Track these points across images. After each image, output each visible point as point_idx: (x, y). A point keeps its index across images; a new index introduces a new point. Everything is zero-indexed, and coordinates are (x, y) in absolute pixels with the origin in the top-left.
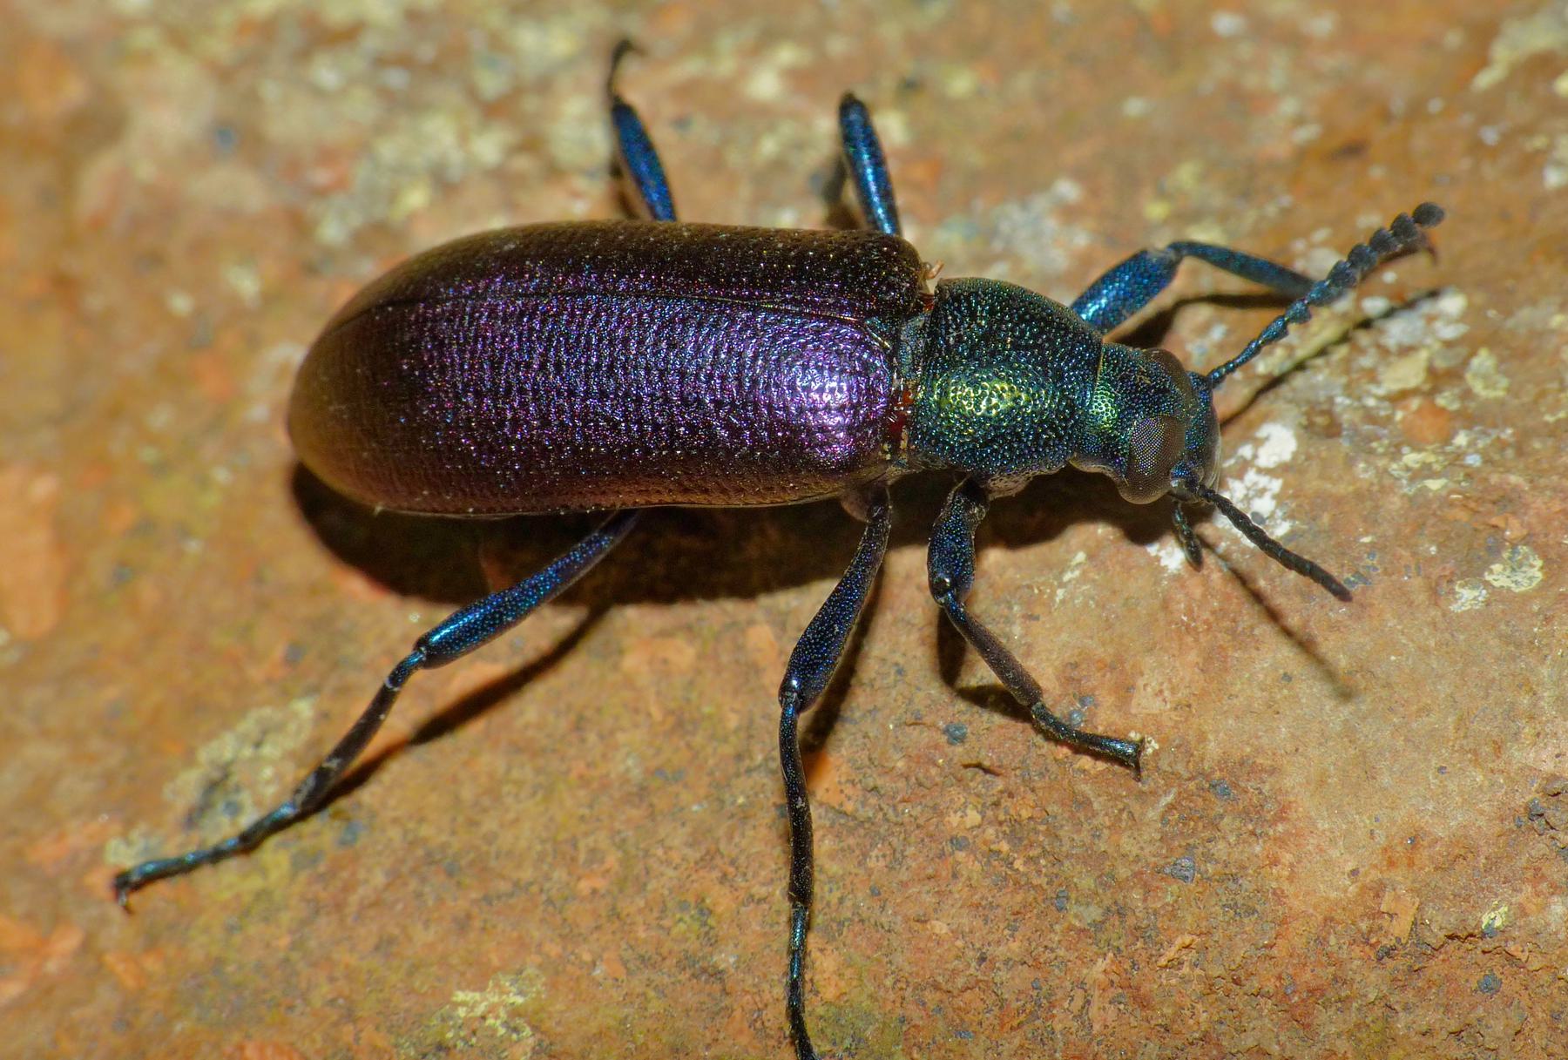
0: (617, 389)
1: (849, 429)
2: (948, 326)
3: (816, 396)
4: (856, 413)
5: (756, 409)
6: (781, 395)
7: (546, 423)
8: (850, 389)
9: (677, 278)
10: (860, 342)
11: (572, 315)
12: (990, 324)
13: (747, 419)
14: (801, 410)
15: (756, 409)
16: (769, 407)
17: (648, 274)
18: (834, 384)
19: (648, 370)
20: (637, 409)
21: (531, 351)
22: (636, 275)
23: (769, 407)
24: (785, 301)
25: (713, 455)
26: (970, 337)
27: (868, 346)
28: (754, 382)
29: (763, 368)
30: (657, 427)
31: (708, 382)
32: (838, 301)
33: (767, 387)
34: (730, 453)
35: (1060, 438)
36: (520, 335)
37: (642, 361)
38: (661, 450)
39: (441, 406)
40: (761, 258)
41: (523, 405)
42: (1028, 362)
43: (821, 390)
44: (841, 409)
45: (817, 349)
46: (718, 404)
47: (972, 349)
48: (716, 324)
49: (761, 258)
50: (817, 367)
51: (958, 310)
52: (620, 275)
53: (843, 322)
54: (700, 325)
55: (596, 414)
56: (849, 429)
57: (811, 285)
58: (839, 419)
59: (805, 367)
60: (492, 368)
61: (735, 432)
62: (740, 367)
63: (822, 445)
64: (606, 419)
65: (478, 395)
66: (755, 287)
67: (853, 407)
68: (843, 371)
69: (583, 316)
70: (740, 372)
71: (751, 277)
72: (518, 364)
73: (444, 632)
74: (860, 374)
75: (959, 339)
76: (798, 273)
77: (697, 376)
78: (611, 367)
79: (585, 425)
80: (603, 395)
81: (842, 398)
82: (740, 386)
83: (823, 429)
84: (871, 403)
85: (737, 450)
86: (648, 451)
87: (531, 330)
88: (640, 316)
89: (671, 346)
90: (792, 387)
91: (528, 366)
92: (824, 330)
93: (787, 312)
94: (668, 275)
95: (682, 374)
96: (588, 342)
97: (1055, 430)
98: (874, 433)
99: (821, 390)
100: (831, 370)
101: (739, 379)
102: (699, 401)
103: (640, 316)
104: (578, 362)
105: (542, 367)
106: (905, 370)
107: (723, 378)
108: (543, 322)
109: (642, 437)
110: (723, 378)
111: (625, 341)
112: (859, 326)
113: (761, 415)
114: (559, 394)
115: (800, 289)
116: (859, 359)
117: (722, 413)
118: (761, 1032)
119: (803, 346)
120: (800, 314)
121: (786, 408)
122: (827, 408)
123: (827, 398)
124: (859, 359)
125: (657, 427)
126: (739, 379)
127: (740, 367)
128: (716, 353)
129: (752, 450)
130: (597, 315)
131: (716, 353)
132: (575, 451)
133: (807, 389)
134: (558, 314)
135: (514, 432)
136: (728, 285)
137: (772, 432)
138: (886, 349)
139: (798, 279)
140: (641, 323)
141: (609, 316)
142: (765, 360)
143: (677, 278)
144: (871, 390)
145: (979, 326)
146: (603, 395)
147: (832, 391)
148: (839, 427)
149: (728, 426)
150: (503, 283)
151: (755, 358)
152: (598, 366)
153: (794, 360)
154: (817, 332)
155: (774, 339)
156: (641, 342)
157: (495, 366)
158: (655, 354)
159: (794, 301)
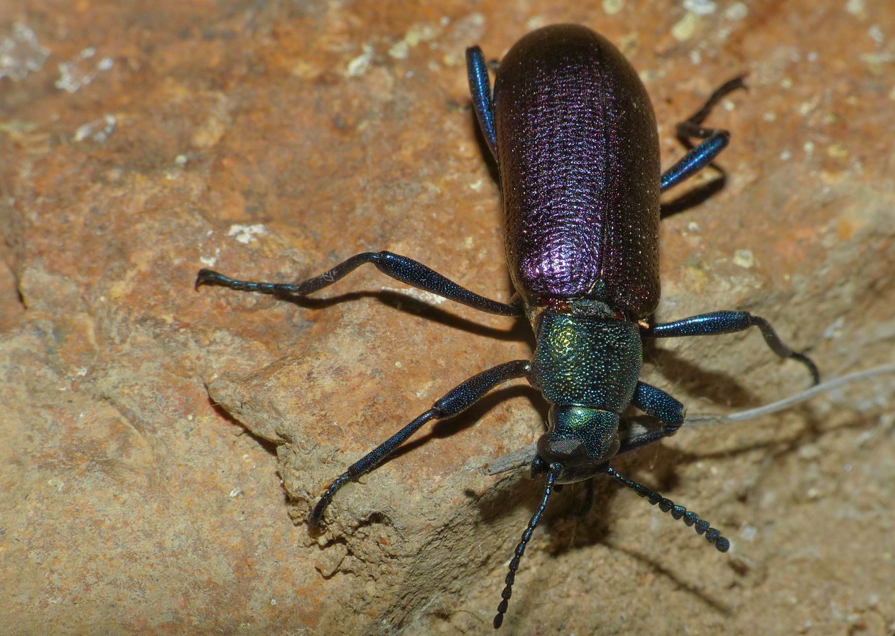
0: (555, 157)
1: (541, 275)
2: (612, 328)
3: (557, 255)
4: (550, 278)
5: (548, 226)
6: (556, 238)
7: (535, 126)
8: (563, 273)
9: (619, 183)
10: (590, 277)
11: (594, 132)
12: (617, 349)
13: (542, 223)
14: (549, 249)
15: (548, 226)
16: (550, 233)
17: (619, 168)
18: (564, 264)
19: (566, 171)
20: (545, 169)
21: (573, 114)
22: (619, 162)
23: (550, 233)
24: (609, 237)
25: (524, 210)
26: (608, 339)
27: (588, 281)
28: (562, 224)
29: (570, 228)
30: (536, 180)
31: (561, 201)
32: (612, 264)
33: (559, 231)
34: (525, 218)
35: (561, 393)
36: (581, 108)
37: (570, 168)
38: (525, 184)
39: (544, 77)
40: (635, 225)
41: (545, 114)
42: (599, 370)
43: (560, 258)
44: (551, 269)
45: (583, 254)
46: (549, 208)
47: (602, 340)
48: (592, 202)
49: (635, 225)
50: (572, 255)
51: (622, 332)
52: (618, 156)
53: (599, 268)
54: (591, 194)
55: (541, 149)
56: (541, 275)
57: (621, 251)
58: (546, 269)
59: (572, 249)
60: (563, 97)
61: (535, 218)
62: (570, 216)
63: (532, 261)
64: (539, 154)
65: (549, 93)
66: (616, 222)
67: (553, 275)
68: (571, 267)
69: (593, 137)
70: (567, 216)
71: (622, 220)
72: (566, 109)
73: (696, 320)
74: (572, 277)
75: (606, 333)
76: (626, 244)
77: (564, 195)
78: (566, 153)
79: (536, 146)
80: (551, 151)
81: (557, 269)
82: (559, 217)
83: (539, 262)
84: (556, 285)
85: (527, 220)
86: (524, 177)
87: (585, 113)
88: (595, 165)
89: (579, 181)
90: (561, 243)
91: (565, 114)
92: (594, 257)
93: (603, 238)
94: (619, 178)
95: (564, 188)
96: (579, 141)
97: (565, 390)
98: (541, 289)
99: (560, 258)
100: (572, 262)
101: (563, 217)
102: (550, 199)
103: (595, 165)
104: (568, 137)
105: (565, 120)
106: (578, 303)
107: (564, 209)
108: (589, 118)
109: (531, 173)
110: (564, 209)
111: (580, 159)
112: (598, 276)
113: (545, 229)
114: (550, 130)
115: (617, 245)
116: (580, 277)
117: (545, 210)
118: (315, 320)
119: (584, 247)
120: (602, 244)
121: (549, 241)
122: (551, 262)
123: (557, 261)
124: (580, 277)
125: (536, 180)
126: (563, 217)
127: (570, 216)
128: (577, 203)
129: (527, 228)
130: (594, 144)
131: (577, 203)
132: (523, 143)
133: (560, 251)
134: (594, 126)
135: (531, 112)
136: (616, 210)
137: (536, 237)
138: (588, 290)
139: (622, 244)
140: (590, 165)
141: (594, 150)
142: (574, 229)
143: (619, 183)
144: (563, 284)
145: (615, 343)
146: (551, 151)
147: (560, 263)
148: (541, 269)
149: (538, 215)
150: (611, 100)
151: (574, 223)
152: (566, 147)
153: (575, 243)
154: (592, 253)
155: (587, 232)
156: (580, 166)
157: (564, 99)
158: (574, 173)
159: (609, 243)
